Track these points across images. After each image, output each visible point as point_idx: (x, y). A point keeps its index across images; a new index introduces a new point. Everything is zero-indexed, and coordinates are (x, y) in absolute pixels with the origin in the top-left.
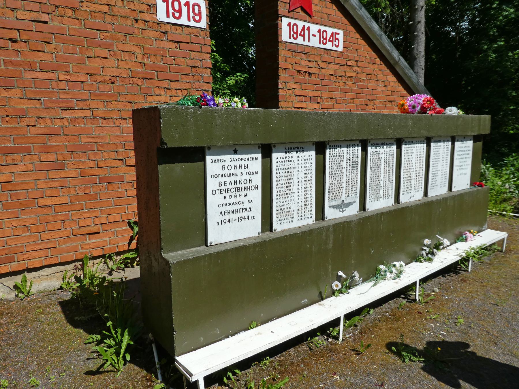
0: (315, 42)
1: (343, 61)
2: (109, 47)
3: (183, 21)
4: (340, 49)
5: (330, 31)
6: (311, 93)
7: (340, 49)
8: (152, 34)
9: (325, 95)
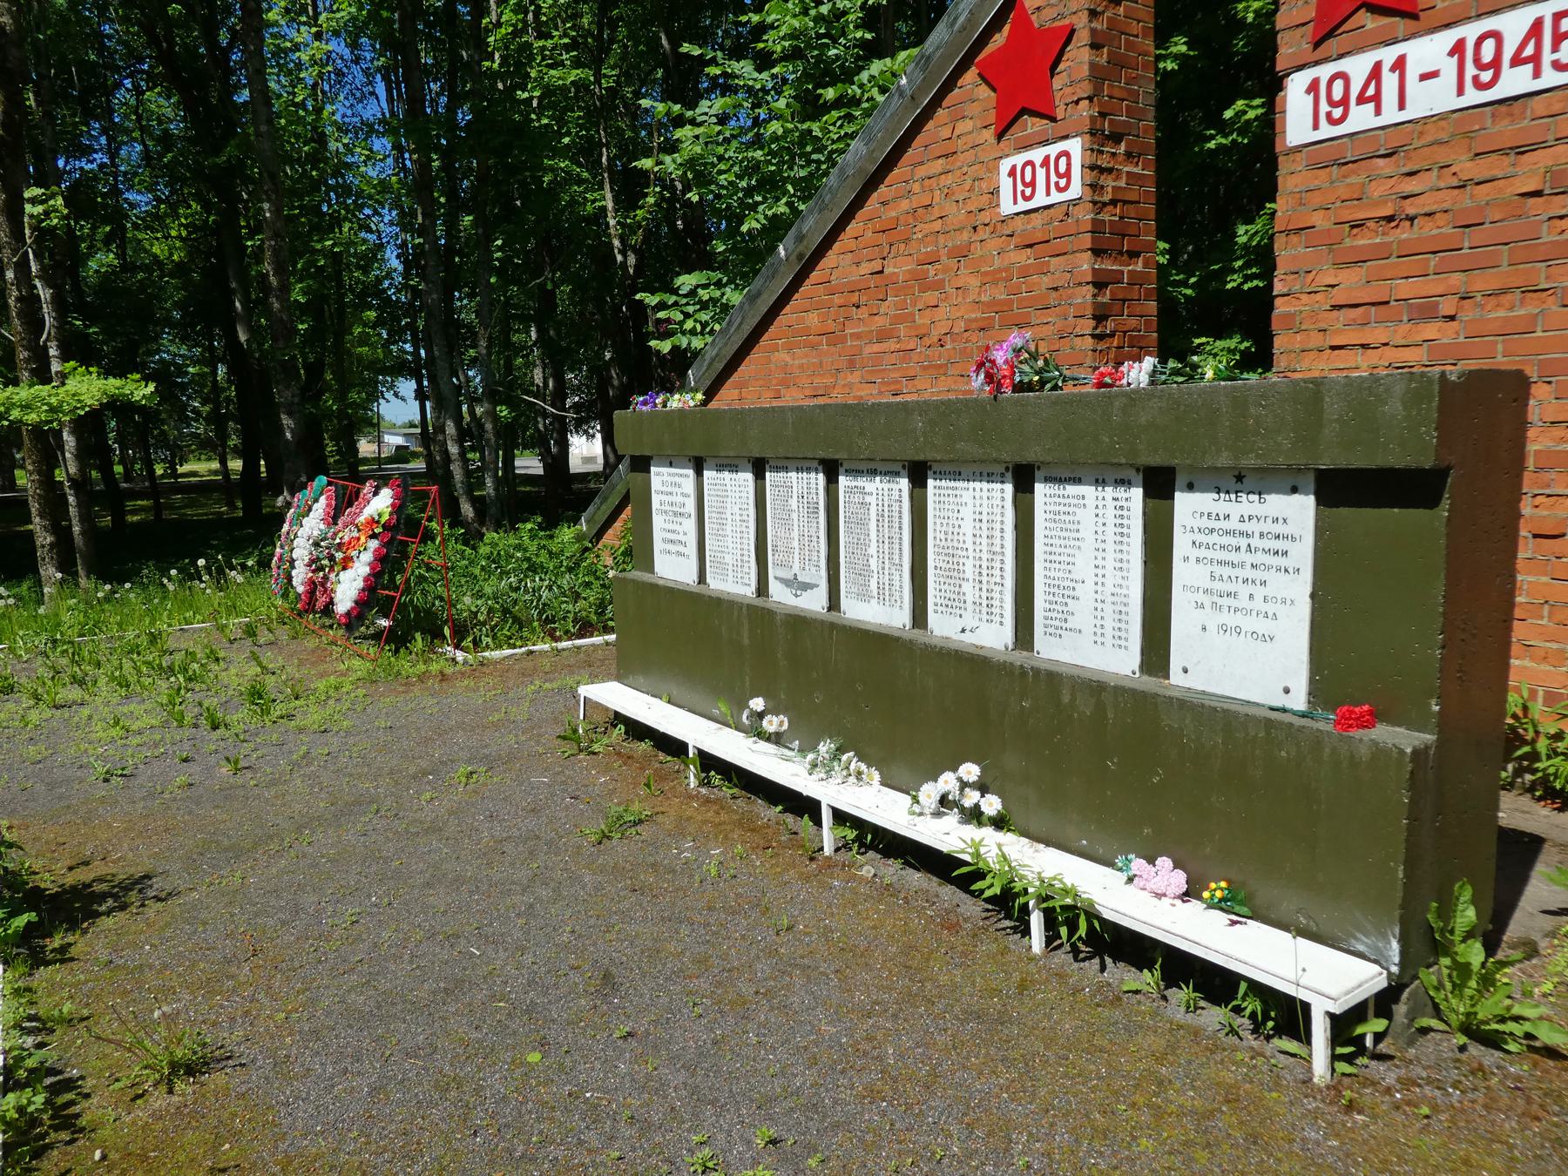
3: (1040, 200)
6: (1404, 288)
9: (1482, 282)
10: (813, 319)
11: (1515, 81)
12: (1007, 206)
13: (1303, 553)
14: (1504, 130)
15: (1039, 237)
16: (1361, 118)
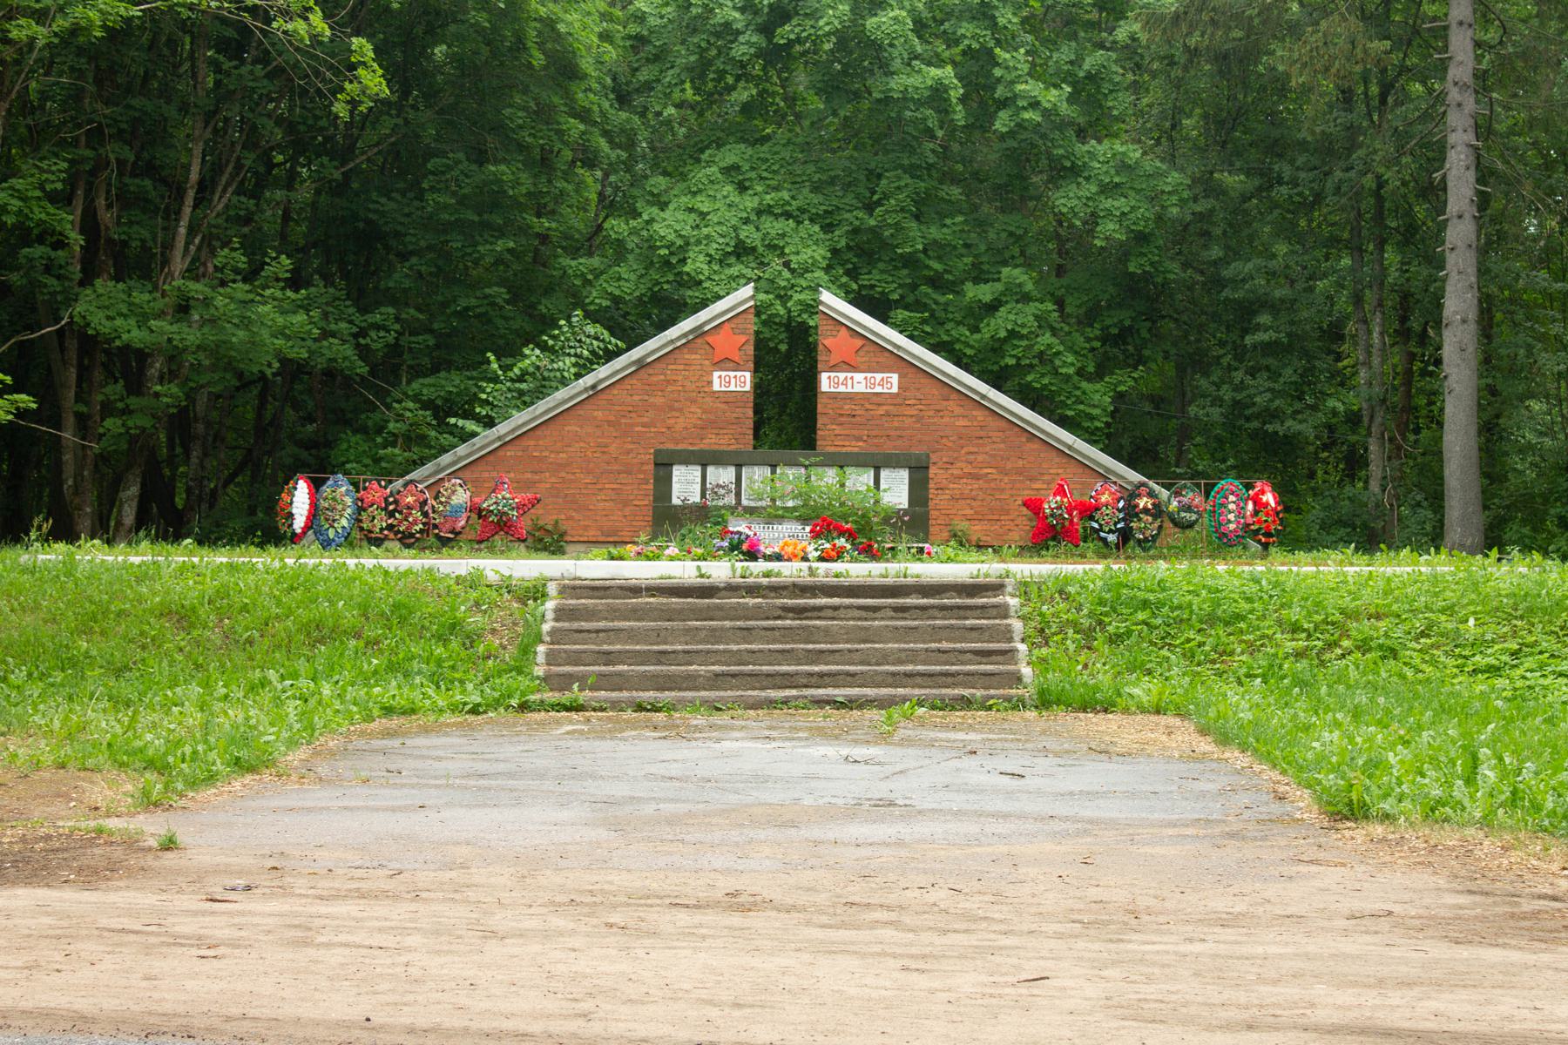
0: (859, 377)
1: (899, 400)
2: (681, 410)
3: (732, 388)
4: (895, 390)
5: (879, 376)
7: (895, 390)
8: (708, 400)
10: (599, 414)
11: (878, 389)
12: (716, 387)
13: (907, 481)
14: (879, 400)
15: (729, 398)
16: (842, 389)
